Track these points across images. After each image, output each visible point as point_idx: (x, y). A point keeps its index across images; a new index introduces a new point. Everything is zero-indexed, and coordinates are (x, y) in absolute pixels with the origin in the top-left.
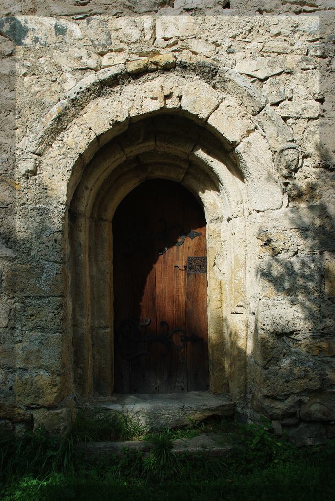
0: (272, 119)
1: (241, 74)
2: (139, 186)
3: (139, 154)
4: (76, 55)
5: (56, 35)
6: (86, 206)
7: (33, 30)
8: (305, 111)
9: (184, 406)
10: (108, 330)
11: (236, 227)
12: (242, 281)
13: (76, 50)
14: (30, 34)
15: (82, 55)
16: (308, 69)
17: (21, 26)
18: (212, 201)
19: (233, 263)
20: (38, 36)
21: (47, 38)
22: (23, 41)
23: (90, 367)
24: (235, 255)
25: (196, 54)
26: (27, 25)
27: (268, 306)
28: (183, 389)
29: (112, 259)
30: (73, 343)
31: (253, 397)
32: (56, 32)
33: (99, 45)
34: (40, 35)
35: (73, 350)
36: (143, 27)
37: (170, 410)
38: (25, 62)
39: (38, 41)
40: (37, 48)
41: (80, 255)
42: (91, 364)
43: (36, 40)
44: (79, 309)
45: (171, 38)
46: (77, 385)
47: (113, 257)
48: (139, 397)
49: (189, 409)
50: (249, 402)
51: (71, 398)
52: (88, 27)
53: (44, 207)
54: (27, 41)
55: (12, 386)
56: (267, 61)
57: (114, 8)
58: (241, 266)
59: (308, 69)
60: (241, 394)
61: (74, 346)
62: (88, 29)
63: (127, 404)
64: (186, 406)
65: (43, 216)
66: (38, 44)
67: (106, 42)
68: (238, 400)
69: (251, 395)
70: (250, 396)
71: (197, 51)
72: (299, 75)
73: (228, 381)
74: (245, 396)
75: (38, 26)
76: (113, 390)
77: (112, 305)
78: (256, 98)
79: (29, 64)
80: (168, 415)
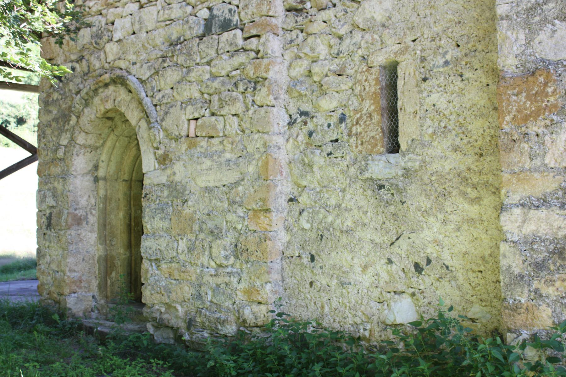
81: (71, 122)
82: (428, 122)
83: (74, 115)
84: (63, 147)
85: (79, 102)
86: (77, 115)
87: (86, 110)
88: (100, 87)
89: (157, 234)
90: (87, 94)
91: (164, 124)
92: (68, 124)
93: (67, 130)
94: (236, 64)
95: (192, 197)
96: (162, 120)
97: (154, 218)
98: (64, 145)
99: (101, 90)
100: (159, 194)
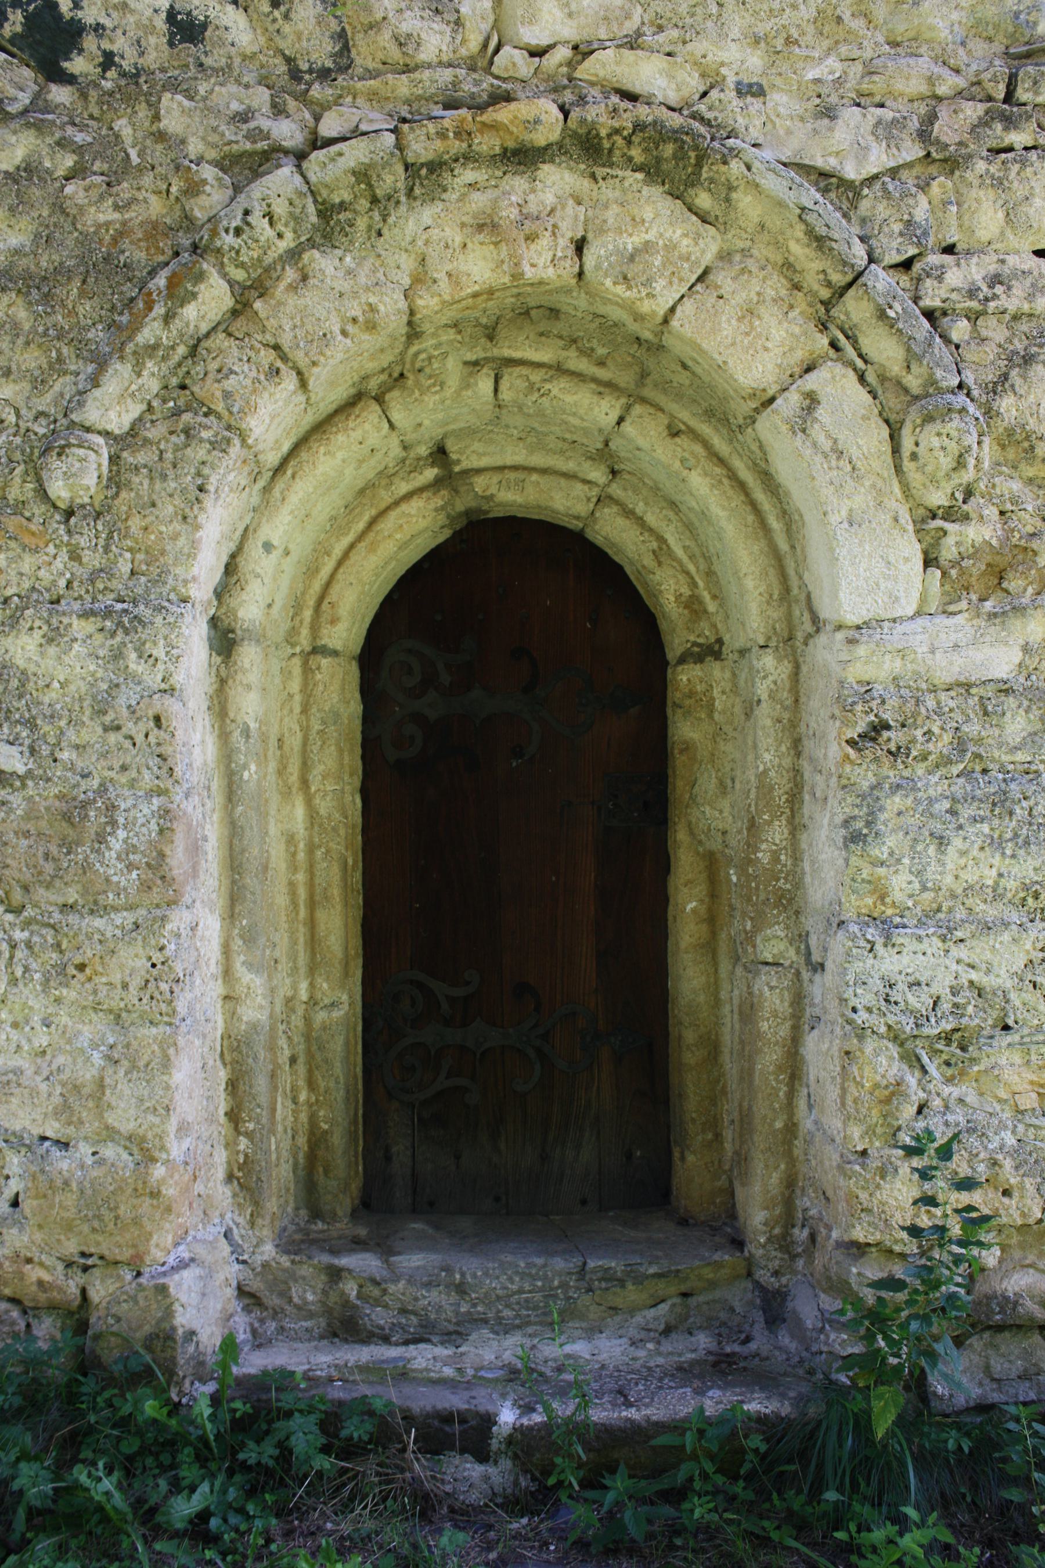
0: (891, 314)
1: (785, 165)
2: (447, 541)
3: (445, 436)
4: (235, 106)
5: (171, 44)
6: (269, 606)
7: (98, 29)
8: (999, 289)
9: (585, 1264)
10: (337, 1014)
11: (765, 677)
12: (783, 857)
13: (233, 88)
14: (90, 42)
15: (255, 105)
16: (1010, 149)
17: (60, 16)
18: (686, 591)
19: (753, 796)
20: (115, 48)
21: (142, 54)
22: (65, 65)
23: (280, 1128)
24: (761, 768)
25: (632, 97)
26: (80, 14)
27: (869, 946)
28: (584, 1202)
29: (357, 782)
30: (222, 1054)
31: (813, 1237)
32: (172, 35)
33: (310, 71)
34: (119, 44)
35: (223, 1075)
36: (458, 11)
37: (534, 1278)
38: (70, 130)
39: (113, 64)
40: (107, 85)
41: (245, 767)
42: (284, 1119)
43: (108, 60)
44: (240, 943)
45: (551, 47)
46: (237, 1189)
47: (360, 772)
48: (437, 1227)
49: (600, 1275)
50: (798, 1255)
51: (214, 1230)
52: (276, 13)
53: (119, 606)
54: (77, 65)
55: (17, 1194)
56: (871, 120)
57: (1005, 585)
58: (779, 806)
59: (1010, 149)
60: (773, 1228)
61: (225, 1064)
62: (275, 20)
63: (399, 1253)
64: (591, 1264)
65: (120, 637)
66: (112, 74)
67: (334, 62)
68: (764, 1246)
69: (806, 1233)
70: (801, 1235)
71: (637, 88)
72: (981, 166)
73: (731, 1182)
74: (786, 1234)
75: (115, 14)
76: (357, 1202)
77: (672, 859)
78: (833, 244)
79: (80, 138)
80: (530, 1292)
81: (190, 312)
82: (202, 92)
83: (224, 275)
84: (100, 440)
85: (280, 208)
86: (239, 275)
87: (322, 262)
88: (468, 158)
89: (960, 914)
90: (363, 175)
91: (1006, 404)
92: (168, 318)
93: (152, 349)
94: (413, 1261)
95: (939, 1537)
96: (1000, 384)
97: (942, 842)
98: (106, 434)
99: (468, 175)
100: (972, 729)
